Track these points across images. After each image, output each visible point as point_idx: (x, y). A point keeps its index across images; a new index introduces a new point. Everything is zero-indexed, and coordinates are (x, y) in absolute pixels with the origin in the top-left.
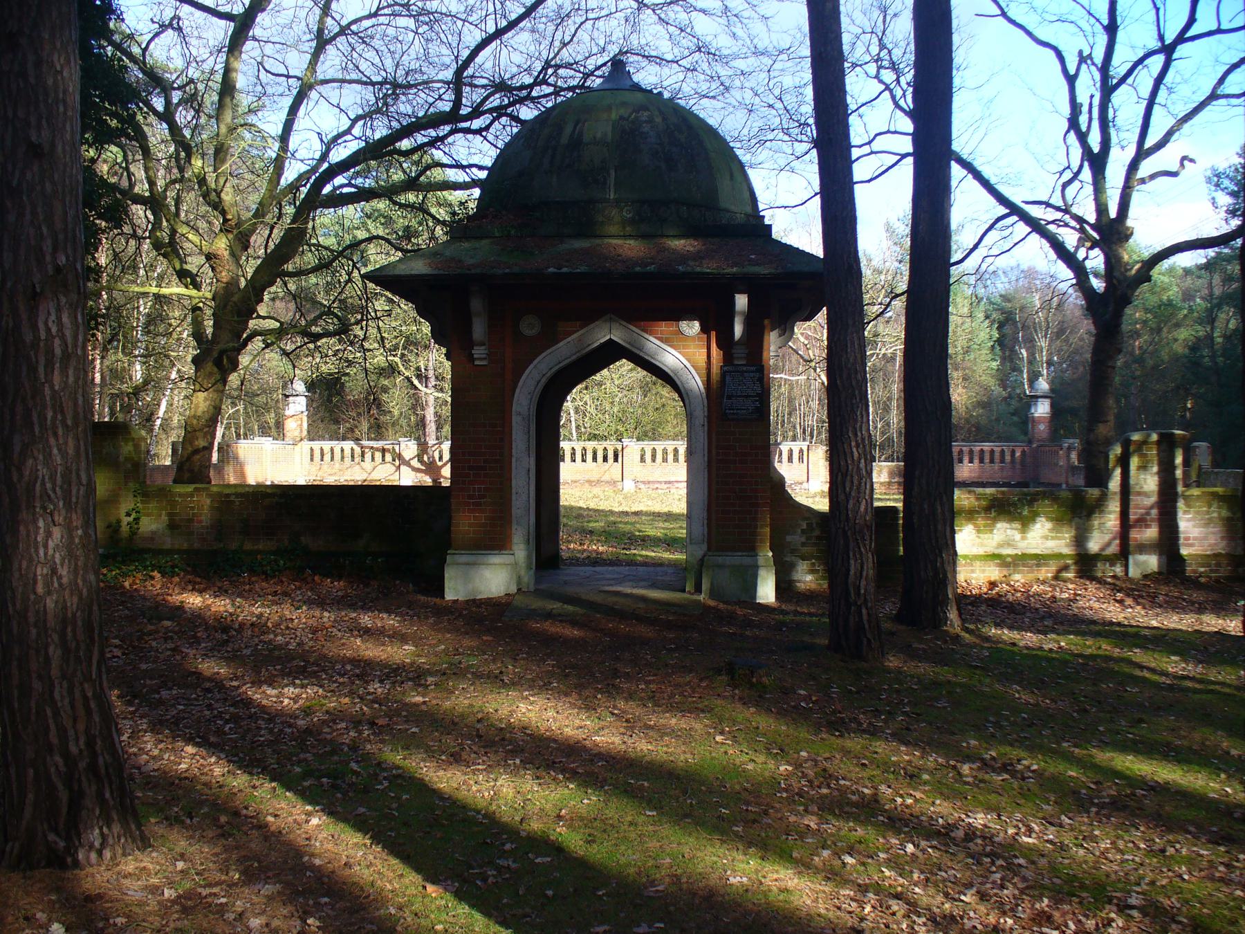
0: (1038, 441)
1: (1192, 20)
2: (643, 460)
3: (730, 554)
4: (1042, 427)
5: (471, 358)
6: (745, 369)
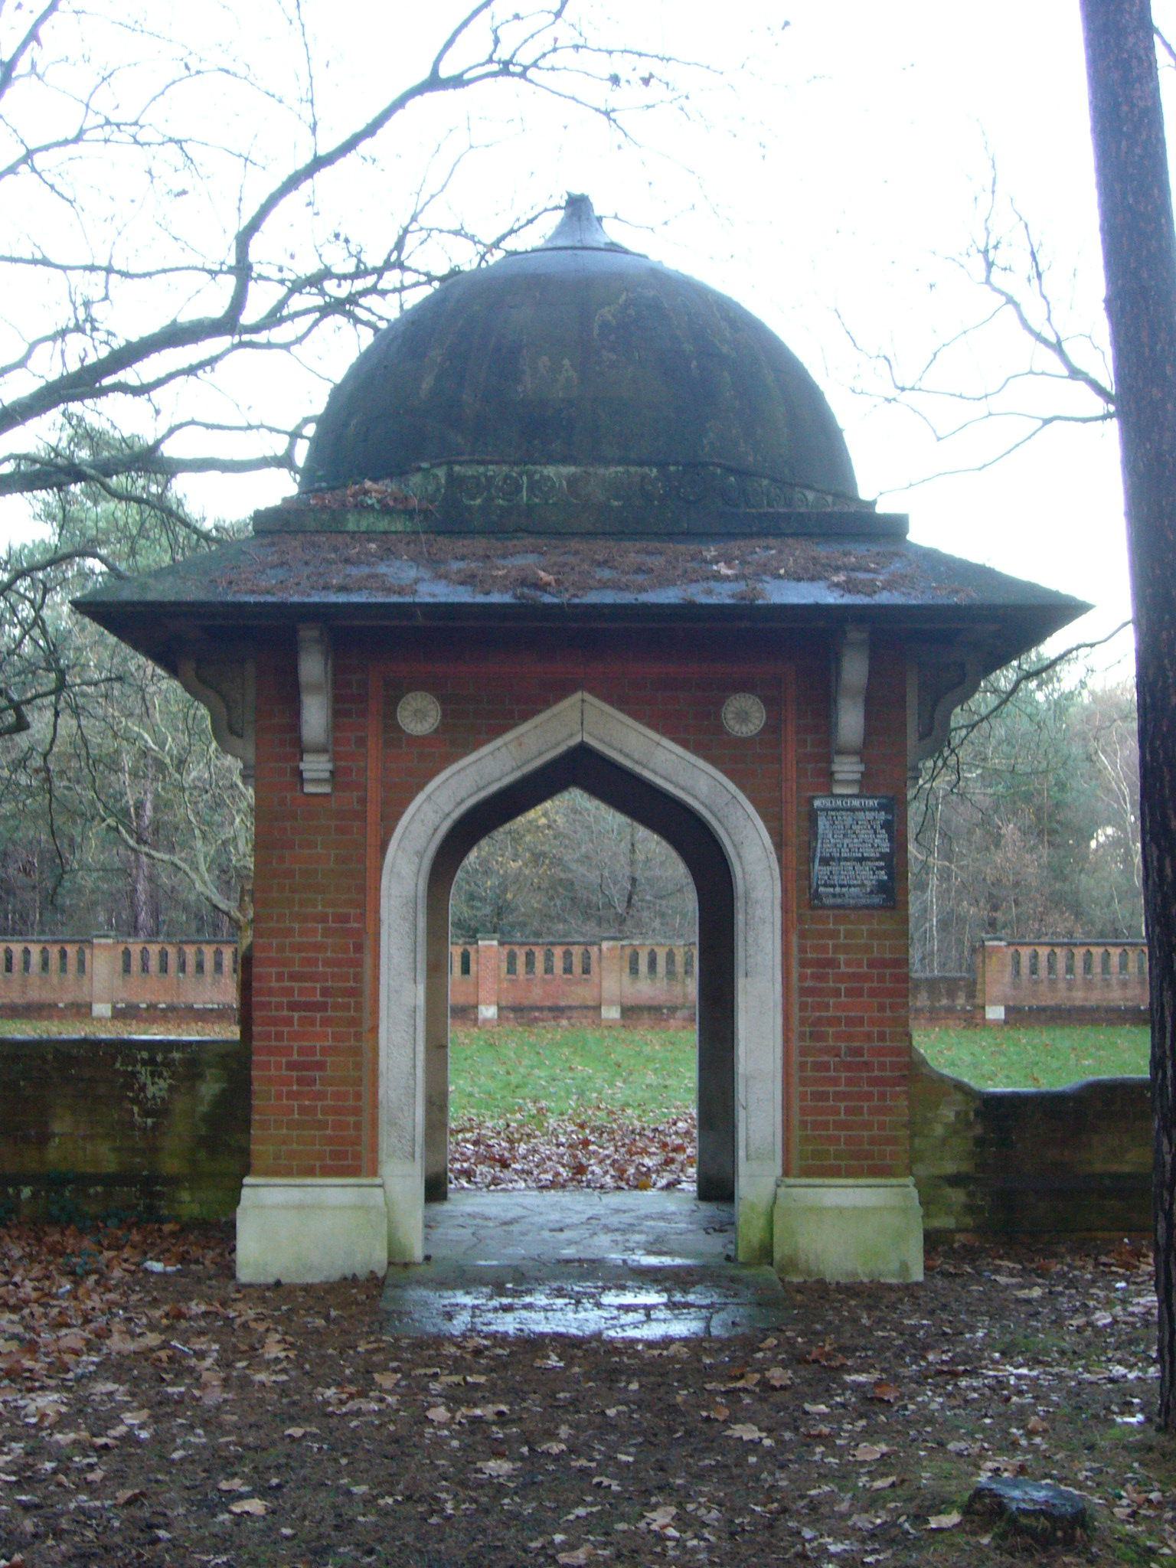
6: (856, 803)
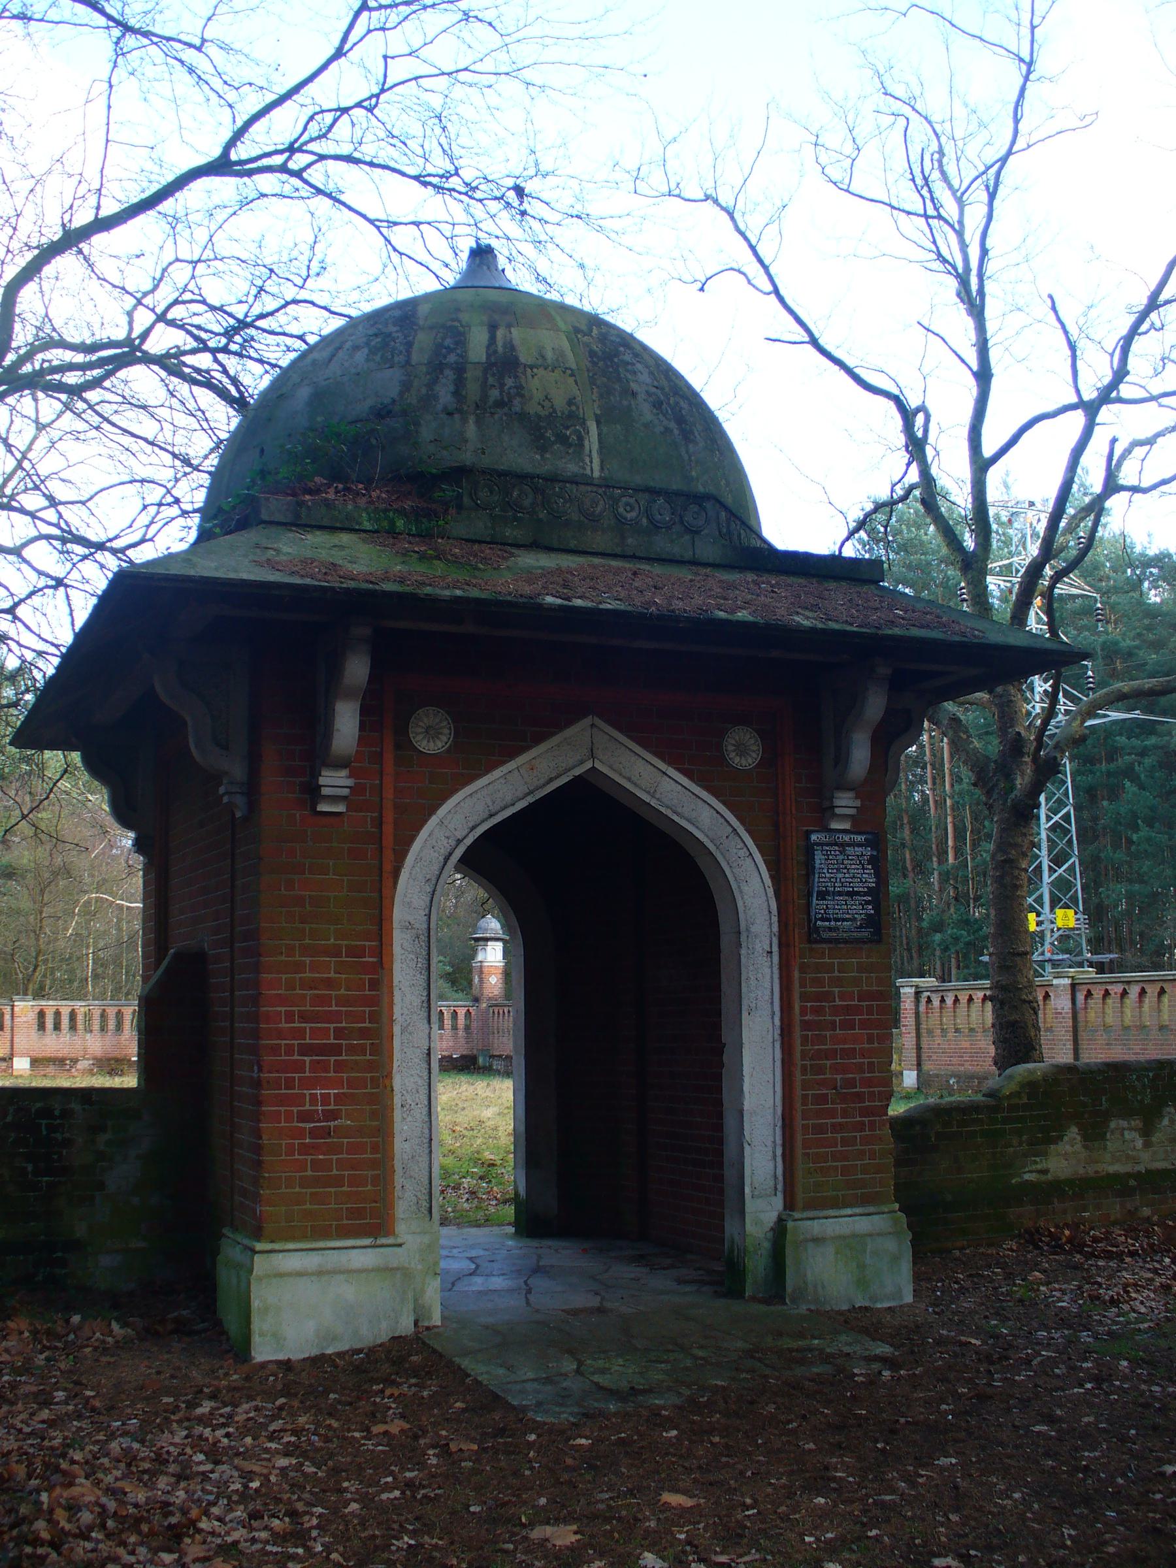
0: (490, 999)
1: (1120, 374)
2: (42, 1026)
3: (832, 1212)
4: (493, 980)
5: (313, 792)
6: (846, 838)
